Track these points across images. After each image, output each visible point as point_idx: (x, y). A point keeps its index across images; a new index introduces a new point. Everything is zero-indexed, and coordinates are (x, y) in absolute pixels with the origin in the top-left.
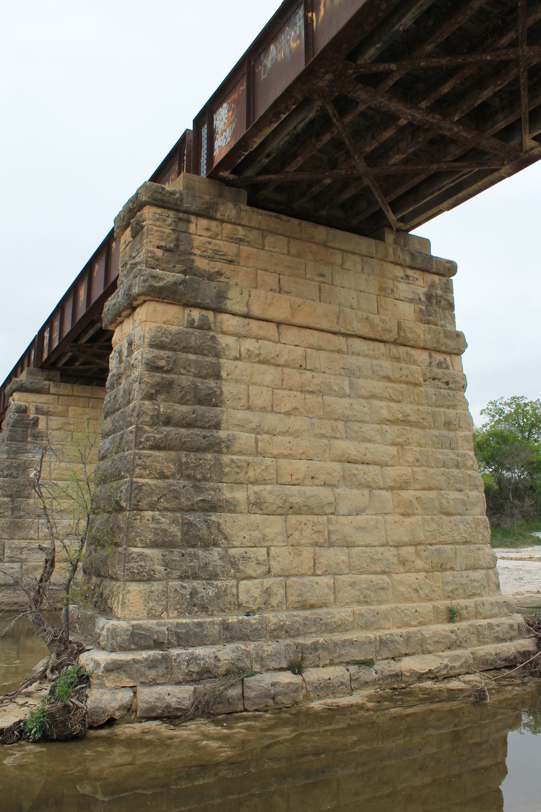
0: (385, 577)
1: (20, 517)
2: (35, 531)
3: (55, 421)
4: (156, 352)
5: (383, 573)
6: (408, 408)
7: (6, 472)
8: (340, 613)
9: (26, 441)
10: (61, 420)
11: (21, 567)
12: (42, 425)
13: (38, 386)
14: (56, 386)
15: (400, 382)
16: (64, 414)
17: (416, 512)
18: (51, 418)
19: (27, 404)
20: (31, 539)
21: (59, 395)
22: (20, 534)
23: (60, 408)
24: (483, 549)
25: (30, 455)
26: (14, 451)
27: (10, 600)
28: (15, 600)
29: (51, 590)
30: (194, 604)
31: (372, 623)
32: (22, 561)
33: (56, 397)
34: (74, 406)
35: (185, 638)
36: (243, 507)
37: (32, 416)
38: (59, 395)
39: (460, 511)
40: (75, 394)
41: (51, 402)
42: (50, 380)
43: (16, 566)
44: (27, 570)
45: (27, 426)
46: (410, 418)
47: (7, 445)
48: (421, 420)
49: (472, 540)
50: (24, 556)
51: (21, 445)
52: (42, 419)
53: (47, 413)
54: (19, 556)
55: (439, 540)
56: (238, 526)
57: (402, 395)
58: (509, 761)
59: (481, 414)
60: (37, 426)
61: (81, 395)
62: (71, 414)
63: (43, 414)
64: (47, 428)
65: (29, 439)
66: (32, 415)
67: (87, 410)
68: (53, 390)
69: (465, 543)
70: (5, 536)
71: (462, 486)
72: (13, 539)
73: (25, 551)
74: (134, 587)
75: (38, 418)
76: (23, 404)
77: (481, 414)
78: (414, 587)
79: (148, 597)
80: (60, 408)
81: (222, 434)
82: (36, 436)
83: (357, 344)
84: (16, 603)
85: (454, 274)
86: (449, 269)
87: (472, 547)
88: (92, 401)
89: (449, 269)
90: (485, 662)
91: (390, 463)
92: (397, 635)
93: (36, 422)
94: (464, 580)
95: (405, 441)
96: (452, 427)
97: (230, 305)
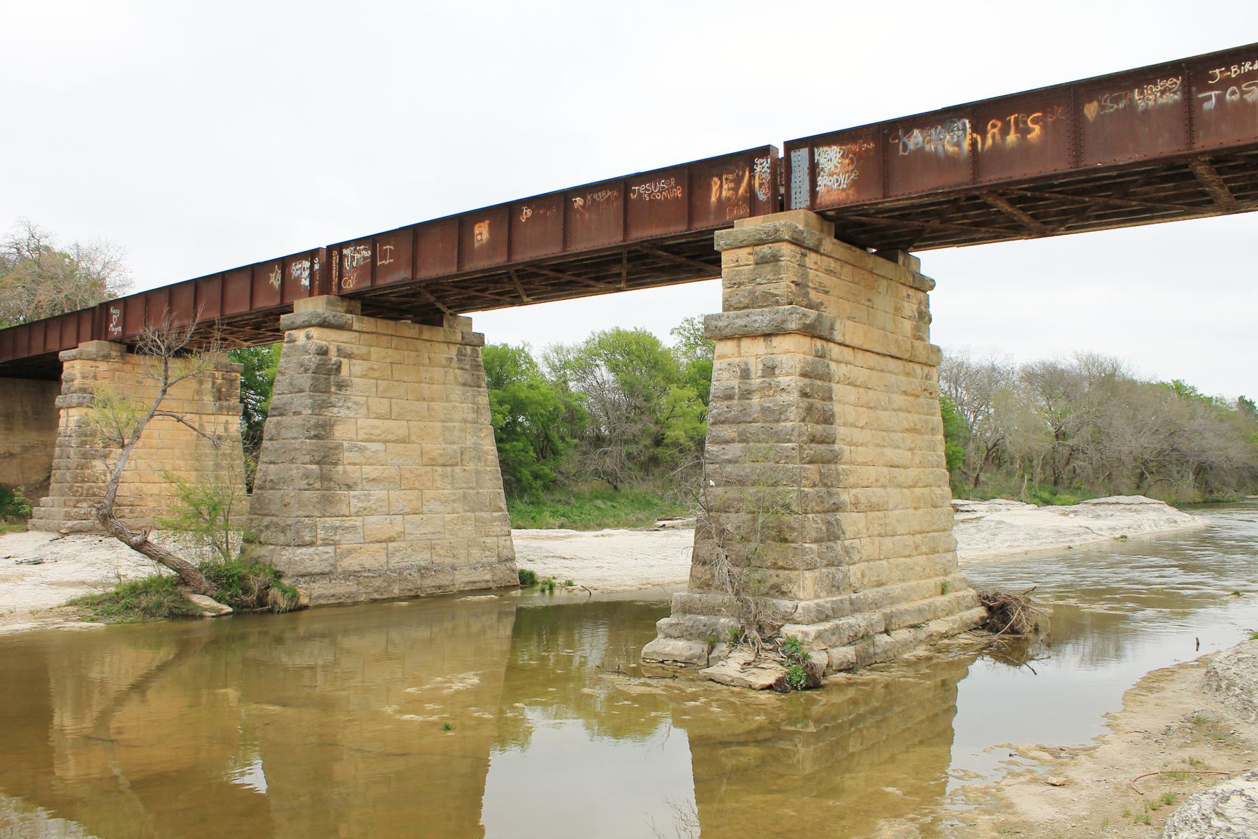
3: (358, 367)
4: (807, 381)
6: (914, 417)
7: (312, 433)
8: (896, 588)
9: (327, 391)
10: (366, 365)
12: (345, 371)
13: (341, 321)
14: (358, 320)
16: (365, 358)
18: (354, 361)
22: (332, 511)
23: (364, 350)
25: (336, 410)
28: (332, 592)
30: (835, 587)
32: (336, 544)
35: (836, 612)
37: (334, 359)
42: (351, 312)
43: (330, 549)
45: (329, 372)
47: (311, 397)
50: (337, 538)
51: (325, 396)
53: (349, 356)
56: (850, 521)
58: (959, 704)
59: (672, 333)
62: (374, 357)
65: (333, 389)
66: (334, 358)
67: (391, 352)
68: (356, 326)
70: (316, 514)
72: (324, 516)
73: (340, 531)
74: (808, 574)
76: (324, 343)
77: (672, 333)
79: (817, 581)
80: (364, 350)
81: (836, 447)
82: (340, 386)
85: (932, 288)
86: (931, 285)
88: (395, 340)
89: (931, 285)
90: (966, 625)
97: (838, 336)
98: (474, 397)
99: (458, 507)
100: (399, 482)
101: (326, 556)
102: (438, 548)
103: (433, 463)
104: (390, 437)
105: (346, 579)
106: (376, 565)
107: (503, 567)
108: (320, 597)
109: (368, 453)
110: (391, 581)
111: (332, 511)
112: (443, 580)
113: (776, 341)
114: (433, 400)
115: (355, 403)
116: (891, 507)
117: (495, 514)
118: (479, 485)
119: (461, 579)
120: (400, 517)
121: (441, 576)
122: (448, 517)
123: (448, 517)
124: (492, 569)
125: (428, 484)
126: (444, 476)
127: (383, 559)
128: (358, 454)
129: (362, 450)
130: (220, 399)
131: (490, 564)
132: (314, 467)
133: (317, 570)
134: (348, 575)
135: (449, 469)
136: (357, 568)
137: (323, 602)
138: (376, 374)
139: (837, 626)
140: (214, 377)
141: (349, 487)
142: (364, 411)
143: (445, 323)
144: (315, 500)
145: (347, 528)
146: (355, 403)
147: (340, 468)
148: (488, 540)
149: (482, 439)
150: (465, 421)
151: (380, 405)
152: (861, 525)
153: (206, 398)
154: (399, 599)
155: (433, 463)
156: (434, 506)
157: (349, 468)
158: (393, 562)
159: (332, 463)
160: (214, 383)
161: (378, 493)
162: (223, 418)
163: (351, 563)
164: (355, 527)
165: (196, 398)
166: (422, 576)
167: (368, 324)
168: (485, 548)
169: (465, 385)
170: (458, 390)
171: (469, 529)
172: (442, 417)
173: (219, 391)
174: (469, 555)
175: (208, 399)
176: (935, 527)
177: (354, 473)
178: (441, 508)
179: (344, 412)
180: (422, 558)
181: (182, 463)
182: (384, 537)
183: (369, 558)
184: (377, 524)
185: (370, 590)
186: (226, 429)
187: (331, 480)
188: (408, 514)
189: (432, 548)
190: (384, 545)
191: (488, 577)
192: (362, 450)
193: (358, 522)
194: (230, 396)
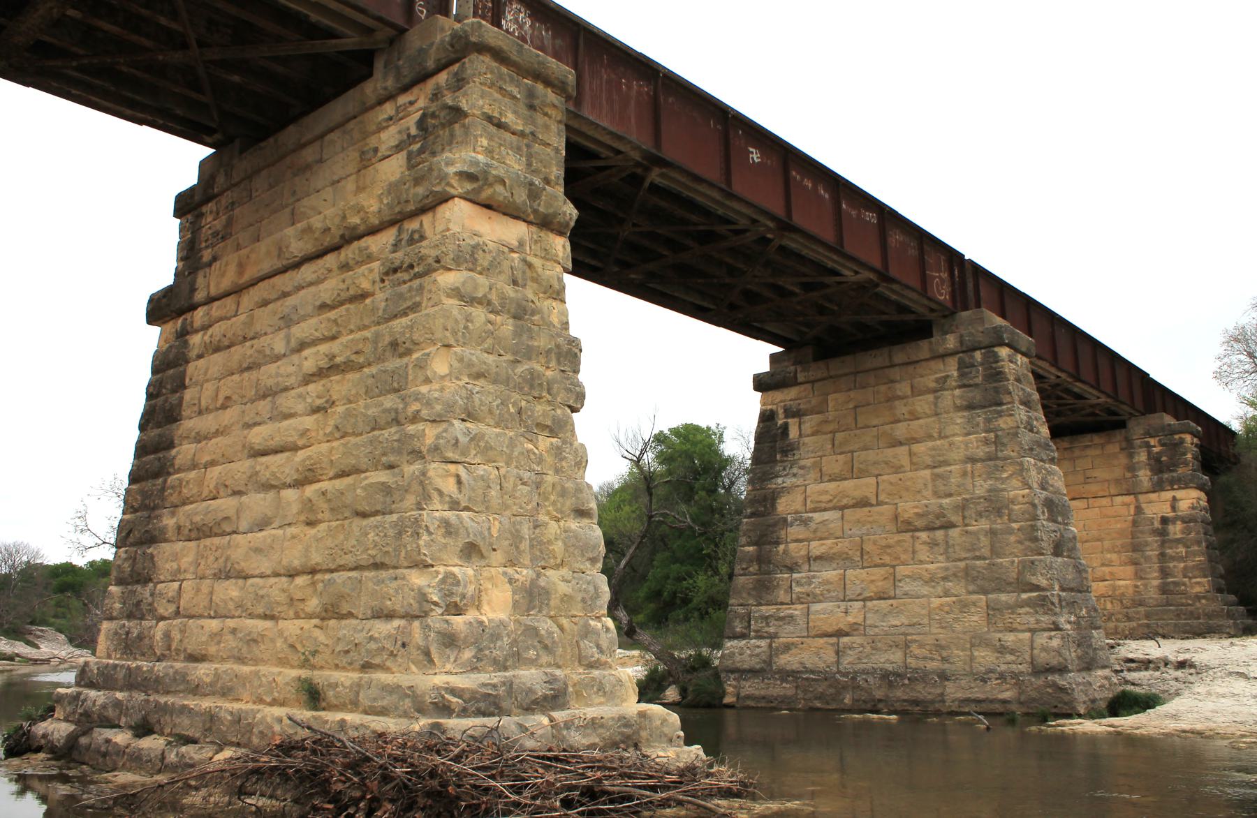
0: (268, 624)
1: (769, 573)
2: (786, 591)
3: (810, 422)
5: (265, 617)
10: (817, 418)
11: (770, 646)
12: (793, 433)
15: (342, 304)
16: (820, 409)
17: (320, 516)
19: (774, 407)
20: (782, 604)
21: (813, 382)
24: (404, 578)
25: (780, 480)
26: (760, 478)
27: (757, 693)
28: (763, 693)
29: (807, 679)
31: (230, 689)
32: (773, 637)
33: (808, 386)
34: (835, 392)
36: (170, 534)
37: (780, 422)
38: (813, 382)
39: (379, 507)
40: (832, 373)
41: (803, 394)
43: (763, 643)
44: (777, 649)
46: (338, 360)
48: (354, 357)
49: (387, 561)
50: (772, 630)
52: (793, 423)
54: (767, 629)
55: (342, 563)
57: (337, 324)
60: (787, 435)
61: (840, 372)
63: (793, 417)
64: (800, 435)
65: (778, 457)
69: (378, 566)
70: (751, 601)
71: (392, 458)
72: (760, 604)
73: (773, 622)
75: (428, 451)
78: (290, 641)
83: (307, 272)
84: (764, 698)
87: (384, 574)
91: (300, 443)
92: (226, 711)
93: (785, 428)
94: (360, 638)
95: (327, 402)
96: (401, 350)
98: (988, 421)
99: (957, 587)
100: (863, 558)
101: (758, 650)
102: (914, 647)
103: (908, 527)
104: (845, 501)
105: (783, 680)
106: (822, 665)
107: (1040, 682)
108: (748, 697)
109: (812, 525)
110: (841, 689)
111: (769, 598)
112: (924, 692)
113: (233, 349)
114: (916, 441)
115: (802, 468)
116: (244, 526)
117: (1024, 596)
118: (995, 552)
119: (954, 692)
120: (859, 604)
121: (919, 687)
122: (936, 602)
123: (936, 602)
124: (1019, 684)
125: (903, 557)
126: (933, 544)
127: (830, 657)
128: (802, 528)
129: (805, 522)
130: (1161, 471)
131: (1015, 675)
132: (751, 548)
133: (746, 667)
134: (785, 675)
135: (939, 534)
136: (796, 666)
137: (752, 704)
138: (831, 427)
139: (343, 721)
140: (1148, 446)
141: (791, 569)
142: (813, 475)
143: (935, 332)
144: (751, 586)
145: (782, 619)
146: (802, 468)
147: (782, 547)
148: (1010, 638)
149: (1004, 481)
150: (972, 460)
151: (834, 464)
152: (186, 561)
153: (1141, 473)
154: (850, 711)
155: (908, 527)
156: (907, 586)
157: (792, 546)
158: (847, 661)
159: (770, 543)
160: (1149, 453)
161: (830, 574)
162: (1168, 495)
163: (786, 661)
164: (791, 616)
165: (1128, 475)
166: (891, 685)
167: (817, 370)
168: (1002, 649)
169: (970, 407)
170: (959, 418)
171: (975, 619)
172: (929, 461)
173: (1158, 460)
174: (972, 658)
175: (1144, 476)
176: (349, 560)
177: (796, 550)
178: (925, 590)
179: (789, 482)
180: (890, 659)
181: (1114, 557)
182: (830, 630)
183: (810, 655)
184: (827, 613)
185: (809, 696)
186: (1174, 508)
187: (770, 562)
188: (871, 599)
189: (907, 645)
190: (834, 640)
191: (1007, 695)
192: (805, 522)
193: (797, 610)
194: (1176, 465)
